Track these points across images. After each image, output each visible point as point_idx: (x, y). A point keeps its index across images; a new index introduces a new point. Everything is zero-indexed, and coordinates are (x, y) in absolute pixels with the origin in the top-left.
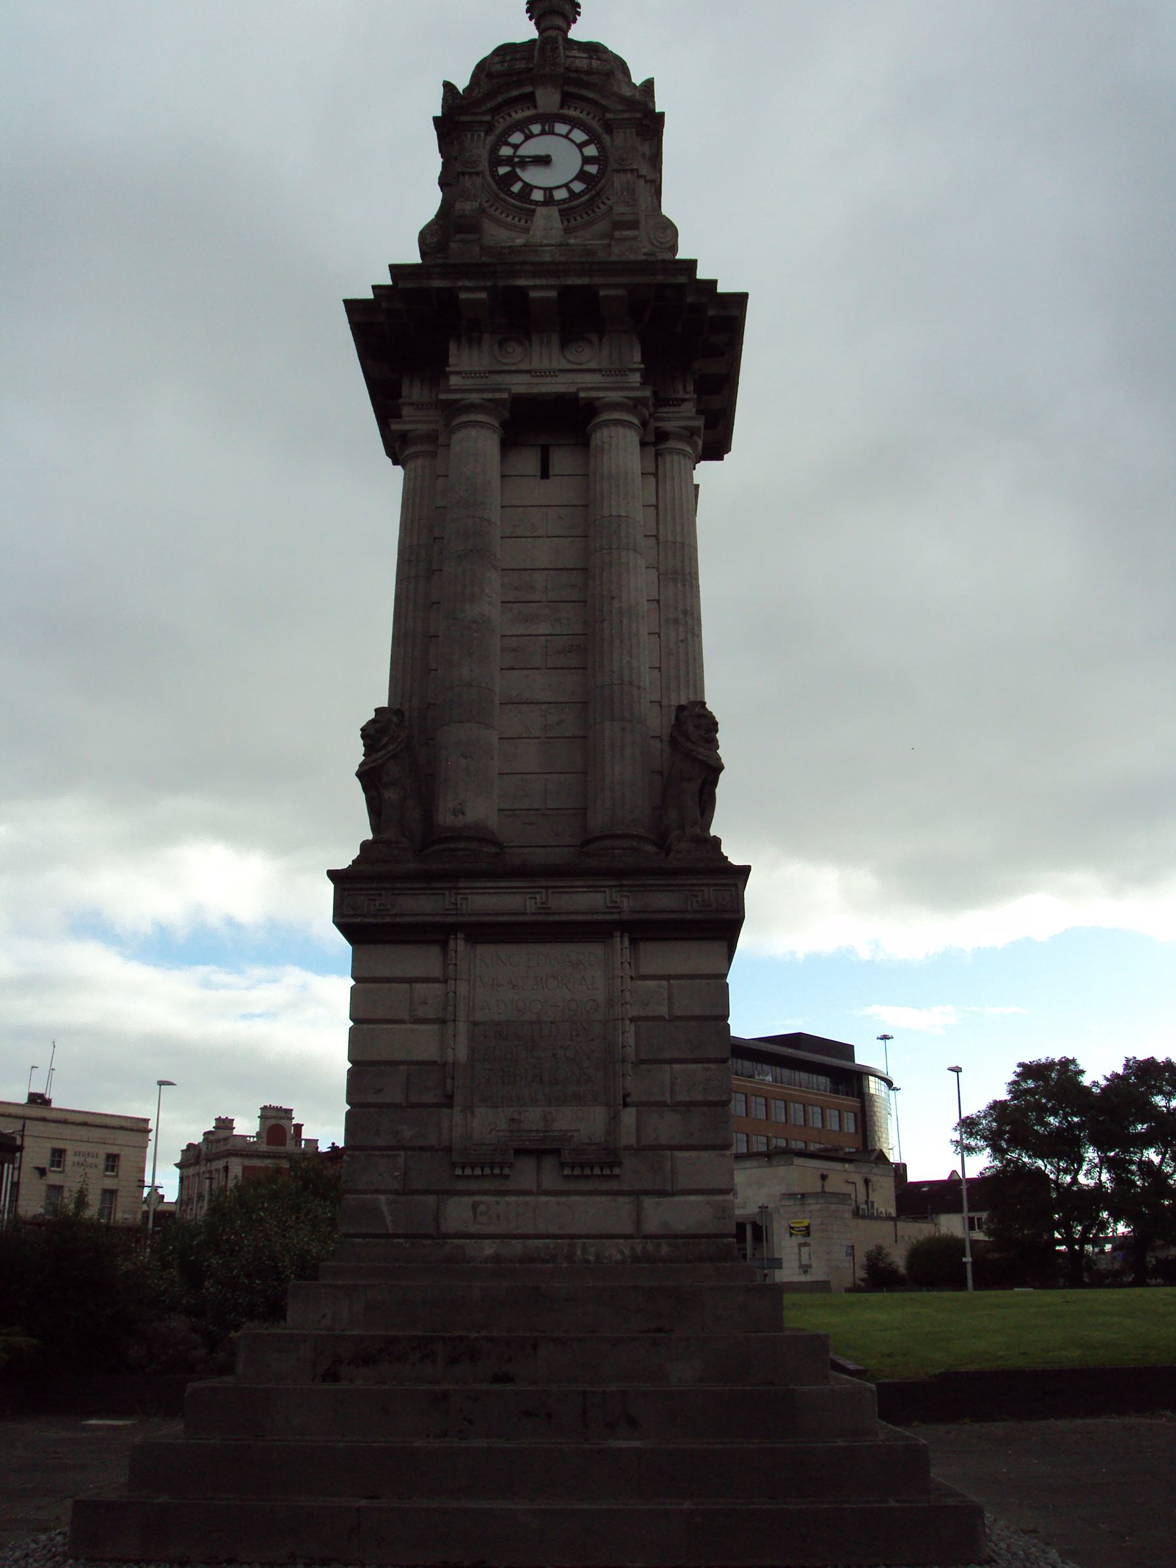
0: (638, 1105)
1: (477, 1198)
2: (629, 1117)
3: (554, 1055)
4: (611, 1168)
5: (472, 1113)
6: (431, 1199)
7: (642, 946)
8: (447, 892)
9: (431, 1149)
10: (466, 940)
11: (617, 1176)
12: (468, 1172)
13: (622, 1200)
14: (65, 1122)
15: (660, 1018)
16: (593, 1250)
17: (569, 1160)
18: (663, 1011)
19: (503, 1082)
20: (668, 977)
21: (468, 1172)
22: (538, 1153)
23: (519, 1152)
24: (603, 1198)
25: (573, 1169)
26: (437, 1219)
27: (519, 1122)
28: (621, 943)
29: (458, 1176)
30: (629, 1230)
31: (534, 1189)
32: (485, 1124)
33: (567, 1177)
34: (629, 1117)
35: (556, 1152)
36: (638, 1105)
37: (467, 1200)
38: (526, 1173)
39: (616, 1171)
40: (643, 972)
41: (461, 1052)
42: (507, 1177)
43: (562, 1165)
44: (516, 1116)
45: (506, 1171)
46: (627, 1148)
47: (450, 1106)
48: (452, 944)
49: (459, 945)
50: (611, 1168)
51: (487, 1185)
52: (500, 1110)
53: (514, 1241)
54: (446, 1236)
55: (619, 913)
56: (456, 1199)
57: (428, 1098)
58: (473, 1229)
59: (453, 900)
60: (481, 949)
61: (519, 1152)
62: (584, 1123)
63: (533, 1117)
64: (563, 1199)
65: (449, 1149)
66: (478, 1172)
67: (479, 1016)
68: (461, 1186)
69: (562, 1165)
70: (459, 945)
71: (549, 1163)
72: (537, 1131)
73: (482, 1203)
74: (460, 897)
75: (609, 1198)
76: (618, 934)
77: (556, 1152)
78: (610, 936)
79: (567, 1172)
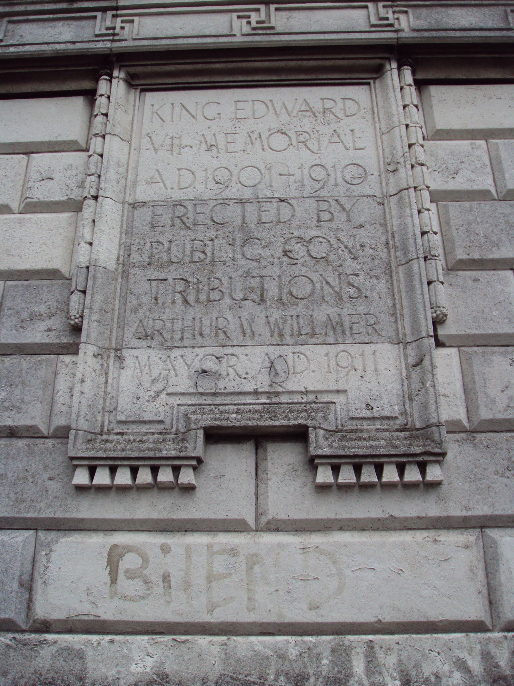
0: (464, 342)
1: (121, 538)
2: (447, 363)
3: (286, 253)
4: (422, 467)
5: (120, 359)
6: (21, 538)
7: (435, 92)
8: (99, 14)
9: (32, 433)
10: (131, 82)
11: (435, 485)
12: (102, 477)
13: (451, 538)
14: (129, 531)
15: (483, 195)
16: (391, 660)
17: (327, 451)
18: (486, 182)
19: (185, 301)
20: (487, 134)
21: (102, 477)
22: (257, 438)
23: (215, 436)
24: (407, 537)
25: (336, 469)
26: (28, 586)
27: (217, 375)
28: (398, 80)
29: (80, 489)
30: (474, 610)
31: (251, 521)
32: (144, 384)
33: (322, 489)
34: (447, 363)
35: (298, 435)
36: (464, 342)
37: (98, 542)
38: (229, 481)
39: (434, 473)
40: (441, 124)
41: (106, 247)
42: (189, 489)
43: (312, 464)
44: (210, 365)
45: (187, 477)
46: (455, 427)
47: (73, 349)
48: (103, 87)
49: (114, 89)
50: (422, 467)
51: (145, 508)
52: (176, 353)
53: (203, 641)
54: (45, 627)
55: (396, 31)
56: (76, 538)
57: (36, 335)
58: (108, 612)
59: (108, 23)
60: (149, 95)
61: (215, 436)
62: (356, 379)
63: (246, 369)
64: (316, 539)
65: (62, 434)
66: (123, 477)
67: (142, 193)
68: (88, 509)
69: (312, 464)
70: (114, 89)
71: (282, 458)
72: (256, 393)
73: (129, 549)
74: (119, 20)
75: (420, 536)
76: (394, 65)
77: (298, 435)
78: (378, 71)
79: (324, 475)
